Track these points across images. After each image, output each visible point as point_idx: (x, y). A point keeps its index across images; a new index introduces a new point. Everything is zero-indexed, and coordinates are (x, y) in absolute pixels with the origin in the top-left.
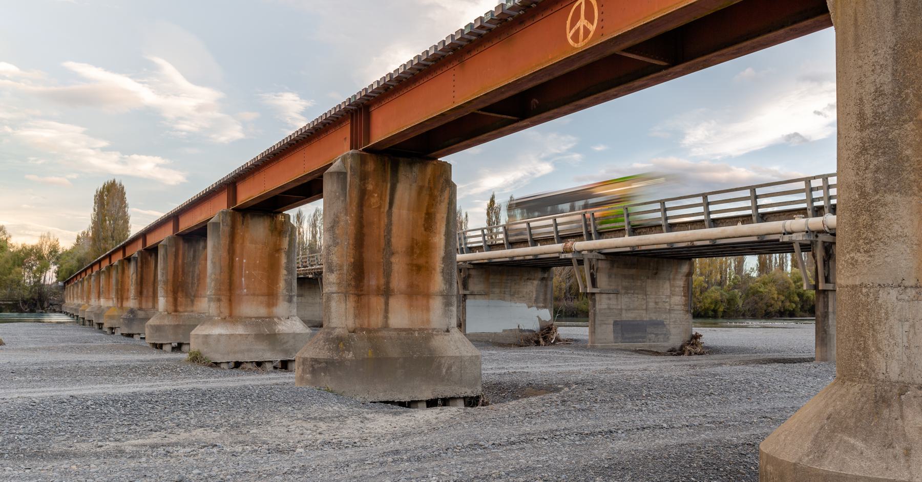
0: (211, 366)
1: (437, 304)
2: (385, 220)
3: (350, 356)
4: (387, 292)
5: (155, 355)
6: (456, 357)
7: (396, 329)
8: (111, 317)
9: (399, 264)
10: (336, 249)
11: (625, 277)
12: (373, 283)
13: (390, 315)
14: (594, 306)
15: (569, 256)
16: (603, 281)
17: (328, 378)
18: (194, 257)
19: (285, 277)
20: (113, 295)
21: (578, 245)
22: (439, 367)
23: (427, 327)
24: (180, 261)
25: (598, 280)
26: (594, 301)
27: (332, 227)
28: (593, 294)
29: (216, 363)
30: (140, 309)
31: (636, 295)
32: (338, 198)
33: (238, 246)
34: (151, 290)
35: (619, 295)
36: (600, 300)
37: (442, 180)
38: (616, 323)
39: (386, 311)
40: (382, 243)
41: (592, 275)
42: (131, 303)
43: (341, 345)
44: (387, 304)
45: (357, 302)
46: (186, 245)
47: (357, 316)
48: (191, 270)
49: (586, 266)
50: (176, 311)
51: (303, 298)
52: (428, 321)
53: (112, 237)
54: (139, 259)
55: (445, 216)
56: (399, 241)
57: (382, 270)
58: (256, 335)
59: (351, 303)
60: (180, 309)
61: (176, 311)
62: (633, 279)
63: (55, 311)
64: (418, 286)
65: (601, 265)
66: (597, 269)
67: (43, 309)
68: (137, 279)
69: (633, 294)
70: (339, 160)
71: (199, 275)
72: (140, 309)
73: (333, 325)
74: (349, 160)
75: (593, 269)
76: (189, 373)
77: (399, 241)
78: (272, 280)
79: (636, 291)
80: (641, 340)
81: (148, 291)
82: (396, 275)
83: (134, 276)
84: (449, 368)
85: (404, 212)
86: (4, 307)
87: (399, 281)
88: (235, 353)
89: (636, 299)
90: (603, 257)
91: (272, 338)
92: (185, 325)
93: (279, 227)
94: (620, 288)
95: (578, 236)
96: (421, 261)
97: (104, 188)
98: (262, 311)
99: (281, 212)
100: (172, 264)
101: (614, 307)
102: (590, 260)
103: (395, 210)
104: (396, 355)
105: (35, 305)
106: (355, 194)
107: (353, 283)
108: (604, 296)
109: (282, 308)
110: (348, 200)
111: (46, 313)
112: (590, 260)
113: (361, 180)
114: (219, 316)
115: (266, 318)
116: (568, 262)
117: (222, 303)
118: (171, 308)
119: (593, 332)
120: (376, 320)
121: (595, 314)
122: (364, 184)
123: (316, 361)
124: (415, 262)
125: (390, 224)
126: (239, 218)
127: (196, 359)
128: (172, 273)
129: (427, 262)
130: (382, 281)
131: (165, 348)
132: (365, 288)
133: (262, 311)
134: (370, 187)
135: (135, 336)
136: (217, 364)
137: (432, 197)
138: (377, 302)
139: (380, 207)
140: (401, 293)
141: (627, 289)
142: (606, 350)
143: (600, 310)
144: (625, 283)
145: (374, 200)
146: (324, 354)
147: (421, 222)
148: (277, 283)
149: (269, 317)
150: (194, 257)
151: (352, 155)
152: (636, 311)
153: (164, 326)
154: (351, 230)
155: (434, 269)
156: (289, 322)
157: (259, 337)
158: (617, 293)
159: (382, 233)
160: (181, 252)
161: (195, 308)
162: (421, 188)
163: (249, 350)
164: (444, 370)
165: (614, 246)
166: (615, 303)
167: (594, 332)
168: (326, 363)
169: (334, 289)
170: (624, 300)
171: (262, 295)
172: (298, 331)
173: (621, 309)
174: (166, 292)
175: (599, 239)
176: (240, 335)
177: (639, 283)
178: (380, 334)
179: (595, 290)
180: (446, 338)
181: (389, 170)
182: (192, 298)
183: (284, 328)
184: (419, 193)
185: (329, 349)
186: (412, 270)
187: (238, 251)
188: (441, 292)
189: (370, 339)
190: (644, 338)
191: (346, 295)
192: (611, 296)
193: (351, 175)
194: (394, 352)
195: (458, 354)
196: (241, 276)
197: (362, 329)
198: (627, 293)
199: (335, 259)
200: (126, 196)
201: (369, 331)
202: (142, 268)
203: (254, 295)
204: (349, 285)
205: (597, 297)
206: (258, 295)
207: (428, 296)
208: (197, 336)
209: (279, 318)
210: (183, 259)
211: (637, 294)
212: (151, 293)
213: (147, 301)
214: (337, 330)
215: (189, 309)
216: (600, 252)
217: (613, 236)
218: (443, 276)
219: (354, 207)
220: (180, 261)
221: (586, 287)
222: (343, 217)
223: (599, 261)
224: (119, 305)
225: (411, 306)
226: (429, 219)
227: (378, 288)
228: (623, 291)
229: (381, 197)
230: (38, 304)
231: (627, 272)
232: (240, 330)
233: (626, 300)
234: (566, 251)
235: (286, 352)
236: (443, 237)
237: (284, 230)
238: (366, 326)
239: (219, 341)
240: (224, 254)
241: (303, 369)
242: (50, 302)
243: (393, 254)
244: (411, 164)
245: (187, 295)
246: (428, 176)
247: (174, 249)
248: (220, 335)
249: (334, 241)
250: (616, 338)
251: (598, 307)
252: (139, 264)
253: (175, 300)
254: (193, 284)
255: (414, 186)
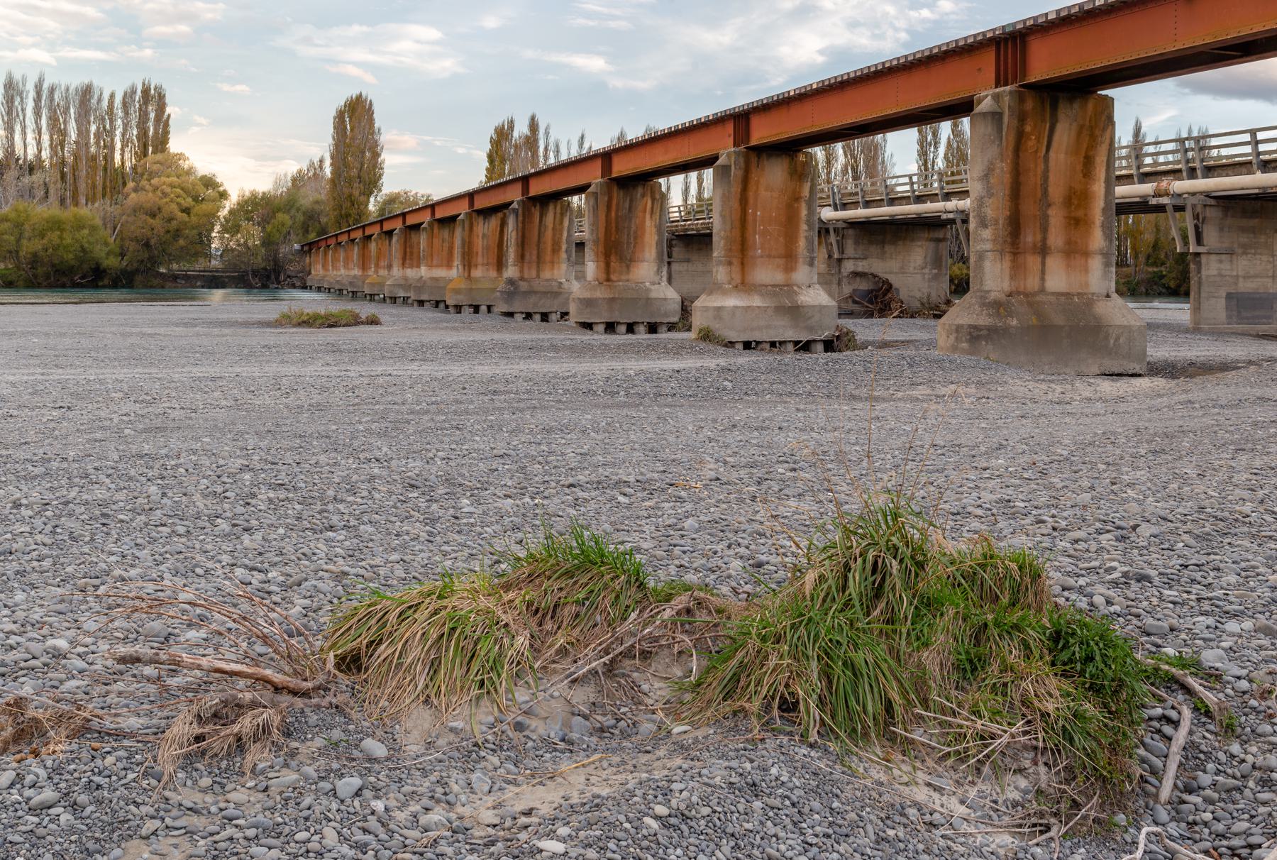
0: (726, 346)
1: (1096, 264)
2: (1042, 166)
3: (1014, 322)
4: (1043, 250)
5: (587, 337)
6: (1125, 326)
7: (1053, 294)
8: (457, 291)
9: (1056, 217)
10: (991, 201)
11: (1243, 230)
12: (1030, 239)
13: (1046, 277)
14: (1199, 272)
15: (1165, 200)
16: (1212, 236)
17: (990, 347)
18: (630, 208)
19: (806, 234)
20: (457, 261)
21: (1180, 186)
22: (1107, 338)
23: (1085, 291)
24: (613, 214)
25: (1205, 235)
26: (1199, 264)
27: (986, 175)
28: (1198, 254)
29: (730, 342)
30: (522, 279)
31: (1258, 257)
32: (993, 142)
33: (751, 194)
34: (535, 252)
35: (1234, 257)
36: (1208, 263)
37: (1104, 118)
38: (1229, 296)
39: (1043, 272)
40: (1039, 195)
41: (1196, 227)
42: (511, 271)
43: (1002, 310)
44: (1043, 264)
45: (1014, 261)
46: (622, 194)
47: (1012, 278)
48: (626, 225)
49: (1188, 215)
50: (608, 280)
51: (690, 265)
52: (1087, 285)
53: (359, 177)
54: (520, 211)
55: (1105, 159)
56: (1056, 191)
57: (1038, 224)
58: (777, 308)
59: (1007, 264)
60: (613, 277)
61: (608, 280)
62: (1254, 232)
63: (294, 286)
64: (1076, 243)
65: (1210, 213)
66: (1204, 219)
67: (279, 283)
68: (517, 239)
69: (1254, 254)
70: (989, 97)
71: (635, 232)
72: (522, 279)
73: (987, 288)
74: (1007, 99)
75: (1198, 219)
76: (701, 353)
77: (1056, 191)
78: (791, 238)
79: (1259, 251)
80: (1264, 320)
81: (531, 254)
82: (1053, 230)
83: (514, 234)
84: (1117, 339)
85: (1062, 156)
86: (226, 280)
87: (1056, 238)
88: (752, 330)
89: (1258, 262)
90: (1213, 202)
91: (795, 312)
92: (621, 299)
93: (799, 169)
94: (1236, 246)
95: (1175, 173)
96: (1080, 213)
97: (345, 106)
98: (779, 277)
99: (800, 150)
100: (604, 217)
101: (1228, 273)
102: (1194, 206)
103: (1052, 154)
104: (1061, 323)
105: (268, 277)
106: (1012, 138)
107: (1009, 240)
108: (1213, 257)
109: (802, 274)
110: (1004, 143)
111: (282, 288)
112: (1194, 206)
113: (1019, 121)
114: (730, 283)
115: (784, 286)
116: (1161, 208)
117: (733, 268)
118: (602, 276)
119: (1197, 310)
120: (1032, 283)
121: (1200, 283)
122: (1022, 126)
123: (975, 327)
124: (1073, 214)
125: (1046, 171)
126: (754, 159)
127: (707, 336)
128: (603, 230)
129: (1086, 215)
130: (1039, 237)
131: (595, 328)
132: (1021, 245)
133: (779, 277)
134: (1028, 128)
135: (516, 315)
136: (731, 344)
137: (1093, 137)
138: (1033, 261)
139: (1036, 152)
140: (1058, 252)
141: (1245, 248)
142: (1219, 334)
143: (1208, 276)
144: (1244, 239)
145: (1031, 143)
146: (984, 320)
147: (1079, 167)
148: (796, 242)
149: (788, 285)
150: (630, 208)
151: (1011, 92)
152: (1259, 280)
153: (596, 299)
154: (1007, 178)
155: (1094, 223)
156: (811, 291)
157: (780, 310)
158: (1231, 253)
159: (1039, 182)
160: (614, 202)
161: (631, 276)
162: (1081, 127)
163: (768, 327)
164: (1112, 341)
165: (1240, 186)
166: (1229, 267)
167: (1199, 309)
168: (988, 330)
169: (988, 246)
170: (1242, 264)
171: (779, 257)
172: (824, 303)
173: (1237, 276)
174: (597, 254)
175: (1207, 177)
176: (758, 307)
177: (1262, 239)
178: (1038, 298)
179: (1200, 249)
180: (1109, 303)
181: (1048, 110)
182: (628, 261)
183: (807, 299)
184: (1079, 133)
185: (990, 315)
186: (1070, 224)
187: (751, 201)
188: (1100, 250)
189: (1030, 304)
190: (1269, 317)
191: (1002, 253)
192: (1223, 257)
193: (1009, 116)
194: (1059, 320)
195: (1126, 323)
196: (755, 233)
197: (1019, 293)
198: (1245, 253)
199: (989, 212)
200: (379, 121)
201: (1026, 295)
202: (523, 222)
203: (769, 256)
204: (1005, 242)
205: (1204, 259)
206: (774, 257)
207: (1086, 254)
208: (706, 309)
209: (799, 287)
210: (617, 211)
211: (1261, 254)
212: (534, 258)
213: (529, 268)
214: (993, 294)
215: (623, 277)
216: (1208, 195)
217: (1230, 173)
218: (1103, 231)
219: (1010, 153)
220: (613, 214)
221: (1186, 243)
222: (999, 165)
223: (1207, 208)
224: (466, 275)
225: (1068, 266)
226: (1088, 162)
227: (1035, 245)
228: (1240, 251)
229: (1038, 140)
230: (273, 277)
231: (1245, 222)
232: (757, 301)
233: (1245, 263)
234: (1157, 194)
235: (811, 329)
236: (1103, 185)
237: (803, 173)
238: (1021, 289)
239: (734, 314)
240: (735, 204)
241: (957, 338)
242: (289, 273)
243: (1049, 205)
244: (1071, 100)
245: (621, 259)
246: (1089, 113)
247: (606, 199)
248: (736, 307)
249: (987, 192)
250: (1229, 317)
251: (1204, 272)
252: (520, 218)
253: (608, 265)
254: (628, 243)
255: (1075, 124)
